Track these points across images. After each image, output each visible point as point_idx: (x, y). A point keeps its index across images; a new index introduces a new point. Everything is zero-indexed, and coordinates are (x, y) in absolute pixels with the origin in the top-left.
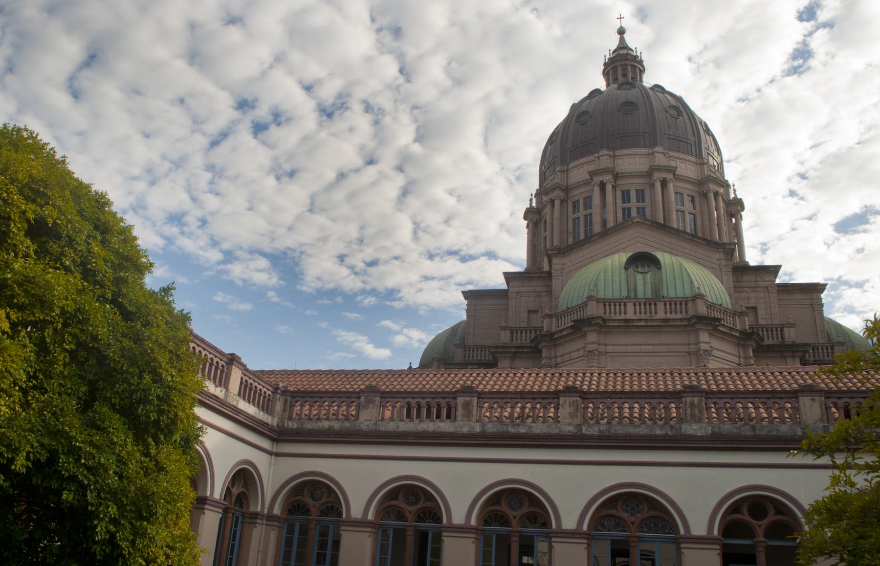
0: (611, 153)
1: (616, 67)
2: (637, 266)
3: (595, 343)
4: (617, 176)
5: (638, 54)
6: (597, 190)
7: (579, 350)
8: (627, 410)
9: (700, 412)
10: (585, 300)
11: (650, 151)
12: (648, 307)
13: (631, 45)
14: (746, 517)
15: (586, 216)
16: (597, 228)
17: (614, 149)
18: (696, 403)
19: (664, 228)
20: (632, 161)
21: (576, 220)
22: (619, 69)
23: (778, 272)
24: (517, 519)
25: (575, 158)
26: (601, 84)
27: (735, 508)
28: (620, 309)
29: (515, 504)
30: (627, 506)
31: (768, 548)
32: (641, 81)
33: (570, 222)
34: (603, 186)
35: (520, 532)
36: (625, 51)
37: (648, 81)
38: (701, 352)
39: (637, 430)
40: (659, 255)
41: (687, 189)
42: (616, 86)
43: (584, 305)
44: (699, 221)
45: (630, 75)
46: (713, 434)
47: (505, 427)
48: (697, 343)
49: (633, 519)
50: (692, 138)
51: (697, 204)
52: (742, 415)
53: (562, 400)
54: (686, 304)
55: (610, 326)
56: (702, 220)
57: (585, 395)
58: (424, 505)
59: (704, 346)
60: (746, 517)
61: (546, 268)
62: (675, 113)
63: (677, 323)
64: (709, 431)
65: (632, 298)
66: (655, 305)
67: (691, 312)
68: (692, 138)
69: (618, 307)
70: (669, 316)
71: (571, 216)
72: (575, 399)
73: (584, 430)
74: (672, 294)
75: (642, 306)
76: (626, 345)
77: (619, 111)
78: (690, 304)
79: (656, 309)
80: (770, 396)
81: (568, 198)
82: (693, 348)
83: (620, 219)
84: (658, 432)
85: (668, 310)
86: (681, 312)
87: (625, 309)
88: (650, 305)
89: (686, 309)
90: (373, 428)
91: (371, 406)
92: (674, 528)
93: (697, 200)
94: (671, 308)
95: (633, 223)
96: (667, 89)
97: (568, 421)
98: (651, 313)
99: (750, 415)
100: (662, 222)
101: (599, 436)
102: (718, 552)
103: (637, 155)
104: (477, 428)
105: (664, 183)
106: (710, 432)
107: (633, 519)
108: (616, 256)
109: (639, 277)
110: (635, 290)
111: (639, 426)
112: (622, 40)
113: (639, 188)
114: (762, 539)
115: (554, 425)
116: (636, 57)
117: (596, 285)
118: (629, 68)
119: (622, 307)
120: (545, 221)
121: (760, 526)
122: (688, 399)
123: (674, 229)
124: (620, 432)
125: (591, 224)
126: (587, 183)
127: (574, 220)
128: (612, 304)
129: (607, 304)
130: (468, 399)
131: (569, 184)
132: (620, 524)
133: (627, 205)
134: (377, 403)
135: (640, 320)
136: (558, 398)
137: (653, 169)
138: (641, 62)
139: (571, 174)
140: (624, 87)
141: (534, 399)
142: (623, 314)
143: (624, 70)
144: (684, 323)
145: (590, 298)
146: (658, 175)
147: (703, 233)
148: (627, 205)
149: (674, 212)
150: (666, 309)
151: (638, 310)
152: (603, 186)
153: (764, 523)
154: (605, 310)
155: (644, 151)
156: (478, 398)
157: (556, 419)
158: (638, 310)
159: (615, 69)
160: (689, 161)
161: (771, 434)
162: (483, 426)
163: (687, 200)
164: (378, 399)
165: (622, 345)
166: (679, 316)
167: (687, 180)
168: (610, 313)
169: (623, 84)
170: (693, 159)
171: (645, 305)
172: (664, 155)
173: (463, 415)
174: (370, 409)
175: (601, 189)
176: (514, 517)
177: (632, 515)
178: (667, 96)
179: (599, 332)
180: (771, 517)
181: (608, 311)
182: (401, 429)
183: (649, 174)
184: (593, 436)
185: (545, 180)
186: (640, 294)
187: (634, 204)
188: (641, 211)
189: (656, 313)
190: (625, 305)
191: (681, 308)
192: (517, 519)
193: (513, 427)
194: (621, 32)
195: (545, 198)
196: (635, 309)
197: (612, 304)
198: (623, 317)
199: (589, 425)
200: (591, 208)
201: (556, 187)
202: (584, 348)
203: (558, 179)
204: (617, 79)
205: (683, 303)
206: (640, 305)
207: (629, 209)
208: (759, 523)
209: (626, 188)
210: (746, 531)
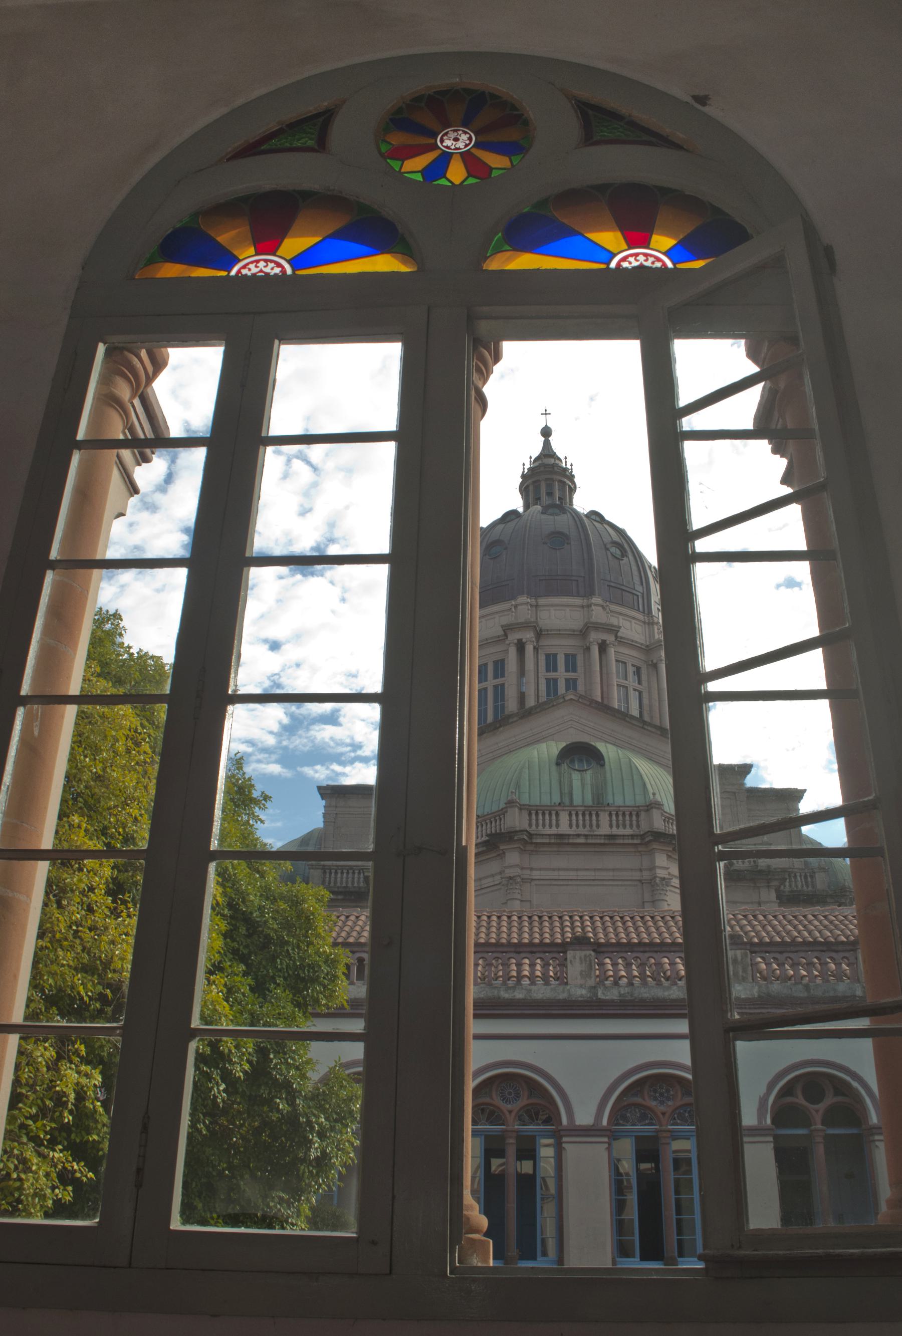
0: (533, 601)
2: (572, 761)
3: (517, 866)
4: (540, 634)
6: (513, 652)
7: (493, 876)
8: (514, 967)
10: (502, 805)
12: (587, 817)
13: (560, 454)
14: (801, 1100)
15: (496, 687)
16: (512, 705)
17: (537, 596)
18: (739, 958)
19: (603, 708)
20: (560, 614)
23: (748, 772)
24: (513, 1114)
26: (517, 503)
27: (788, 1090)
28: (550, 820)
29: (510, 1093)
30: (655, 1091)
34: (521, 647)
35: (517, 1131)
36: (552, 461)
37: (582, 503)
38: (658, 880)
39: (666, 993)
40: (601, 746)
41: (632, 656)
43: (502, 813)
44: (646, 701)
45: (557, 494)
47: (496, 992)
48: (652, 868)
49: (662, 1108)
50: (639, 588)
51: (644, 677)
52: (669, 973)
53: (570, 954)
54: (638, 815)
55: (536, 844)
56: (650, 699)
57: (599, 949)
59: (660, 873)
60: (801, 1100)
62: (618, 552)
63: (626, 841)
64: (756, 992)
65: (566, 804)
66: (597, 815)
67: (644, 827)
68: (639, 588)
69: (547, 817)
70: (615, 831)
72: (588, 953)
73: (600, 995)
74: (619, 801)
75: (580, 817)
76: (559, 869)
77: (545, 543)
78: (643, 815)
79: (598, 821)
80: (825, 949)
82: (646, 875)
85: (614, 822)
86: (631, 826)
87: (557, 821)
88: (590, 815)
89: (638, 821)
93: (644, 671)
94: (617, 821)
98: (591, 826)
99: (678, 972)
101: (621, 1001)
105: (603, 647)
107: (662, 1108)
108: (543, 746)
109: (576, 776)
110: (571, 794)
111: (668, 988)
112: (547, 445)
113: (570, 651)
114: (820, 1127)
115: (561, 988)
116: (566, 469)
117: (518, 786)
119: (554, 817)
121: (817, 1111)
124: (646, 995)
125: (503, 699)
128: (540, 813)
129: (533, 812)
132: (646, 1115)
133: (552, 675)
135: (578, 836)
136: (565, 952)
138: (571, 477)
140: (550, 511)
141: (532, 952)
142: (554, 828)
143: (550, 487)
144: (635, 841)
145: (511, 803)
146: (595, 637)
147: (652, 717)
148: (552, 675)
149: (616, 687)
150: (611, 821)
151: (574, 822)
152: (521, 647)
153: (822, 1106)
154: (530, 820)
155: (578, 601)
157: (562, 979)
158: (574, 822)
163: (631, 670)
165: (553, 870)
166: (628, 831)
167: (631, 645)
168: (537, 825)
171: (584, 815)
172: (603, 607)
176: (510, 1112)
177: (662, 1103)
179: (522, 851)
180: (830, 1100)
181: (534, 822)
183: (583, 633)
184: (613, 1001)
186: (577, 800)
187: (561, 674)
188: (571, 684)
189: (598, 826)
190: (557, 814)
191: (631, 821)
192: (513, 1114)
194: (546, 432)
196: (571, 820)
197: (540, 813)
198: (554, 830)
199: (606, 988)
200: (503, 675)
202: (501, 873)
204: (539, 499)
205: (634, 813)
206: (577, 815)
207: (555, 680)
208: (816, 1106)
209: (553, 651)
210: (802, 1118)
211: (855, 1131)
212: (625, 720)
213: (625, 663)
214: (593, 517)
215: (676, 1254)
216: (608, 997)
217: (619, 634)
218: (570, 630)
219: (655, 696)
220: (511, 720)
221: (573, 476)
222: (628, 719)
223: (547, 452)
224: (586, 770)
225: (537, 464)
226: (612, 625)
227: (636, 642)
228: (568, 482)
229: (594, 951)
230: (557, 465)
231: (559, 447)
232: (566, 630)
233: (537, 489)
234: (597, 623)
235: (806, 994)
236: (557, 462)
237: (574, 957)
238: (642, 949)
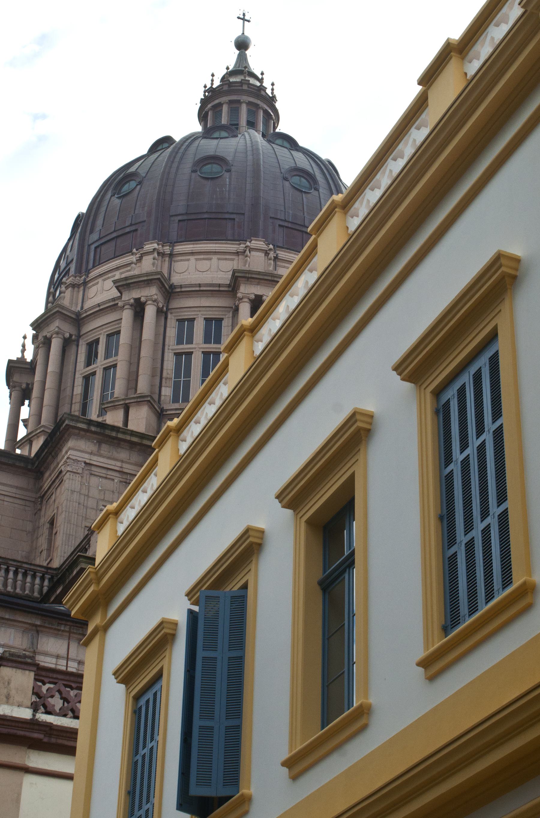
1: (220, 105)
4: (170, 292)
6: (127, 315)
13: (255, 66)
25: (97, 263)
71: (82, 369)
81: (79, 336)
96: (302, 143)
103: (192, 253)
112: (242, 58)
118: (261, 113)
126: (112, 306)
127: (178, 355)
146: (248, 290)
148: (185, 347)
152: (139, 309)
155: (232, 247)
159: (217, 108)
172: (267, 253)
183: (232, 288)
194: (242, 45)
223: (241, 69)
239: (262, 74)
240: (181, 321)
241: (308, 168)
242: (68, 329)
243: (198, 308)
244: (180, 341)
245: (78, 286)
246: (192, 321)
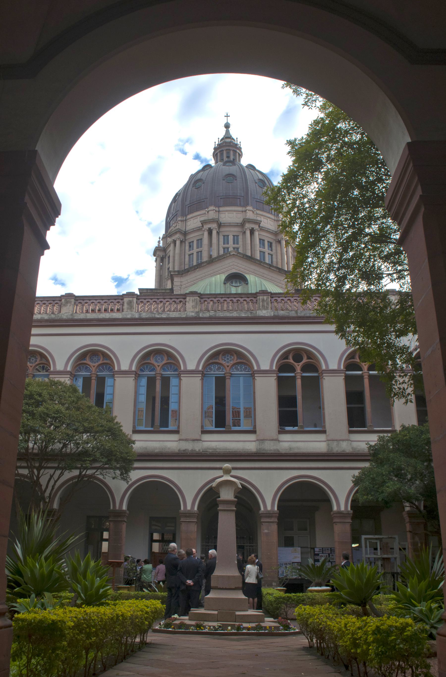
0: (217, 209)
1: (223, 150)
2: (232, 283)
4: (220, 225)
5: (238, 143)
9: (267, 304)
11: (244, 209)
13: (234, 137)
14: (291, 361)
15: (197, 252)
17: (219, 207)
18: (265, 299)
19: (250, 259)
20: (231, 215)
21: (191, 255)
22: (225, 152)
24: (160, 367)
27: (285, 356)
31: (303, 377)
32: (239, 161)
33: (187, 256)
34: (210, 232)
37: (244, 162)
40: (247, 276)
42: (222, 163)
46: (274, 315)
51: (274, 248)
53: (188, 299)
56: (277, 258)
58: (102, 362)
61: (169, 286)
71: (188, 252)
72: (196, 298)
77: (224, 180)
81: (185, 240)
83: (221, 252)
84: (243, 315)
90: (71, 317)
91: (69, 304)
92: (251, 366)
95: (230, 255)
97: (192, 310)
100: (250, 255)
102: (275, 378)
104: (137, 316)
105: (252, 232)
106: (272, 315)
112: (227, 132)
116: (237, 145)
118: (232, 152)
120: (169, 257)
122: (261, 297)
123: (257, 260)
127: (189, 255)
130: (131, 299)
131: (187, 230)
134: (73, 303)
137: (245, 221)
138: (240, 149)
139: (189, 223)
143: (228, 153)
146: (248, 226)
148: (226, 246)
149: (258, 252)
152: (210, 232)
153: (301, 364)
155: (240, 209)
156: (137, 299)
159: (221, 152)
160: (269, 218)
161: (306, 315)
162: (140, 314)
164: (73, 300)
169: (227, 162)
170: (272, 217)
172: (253, 212)
173: (128, 308)
174: (68, 307)
175: (209, 233)
178: (257, 173)
180: (305, 360)
182: (88, 317)
183: (242, 225)
185: (170, 227)
192: (160, 367)
193: (158, 314)
194: (227, 126)
195: (169, 240)
200: (201, 247)
201: (179, 231)
203: (180, 226)
208: (298, 364)
209: (226, 234)
210: (290, 368)
211: (316, 374)
212: (260, 265)
213: (264, 240)
214: (250, 167)
215: (231, 424)
216: (205, 316)
217: (261, 225)
218: (236, 223)
219: (279, 257)
220: (203, 265)
221: (241, 148)
222: (262, 264)
223: (228, 136)
224: (238, 286)
225: (222, 142)
226: (257, 220)
227: (270, 229)
228: (238, 151)
229: (199, 297)
230: (232, 142)
231: (234, 133)
232: (233, 223)
233: (222, 154)
234: (249, 219)
235: (296, 315)
236: (232, 140)
237: (190, 300)
238: (221, 296)
239: (237, 139)
240: (224, 236)
241: (262, 179)
242: (182, 237)
243: (231, 232)
244: (224, 244)
245: (183, 221)
246: (228, 236)
